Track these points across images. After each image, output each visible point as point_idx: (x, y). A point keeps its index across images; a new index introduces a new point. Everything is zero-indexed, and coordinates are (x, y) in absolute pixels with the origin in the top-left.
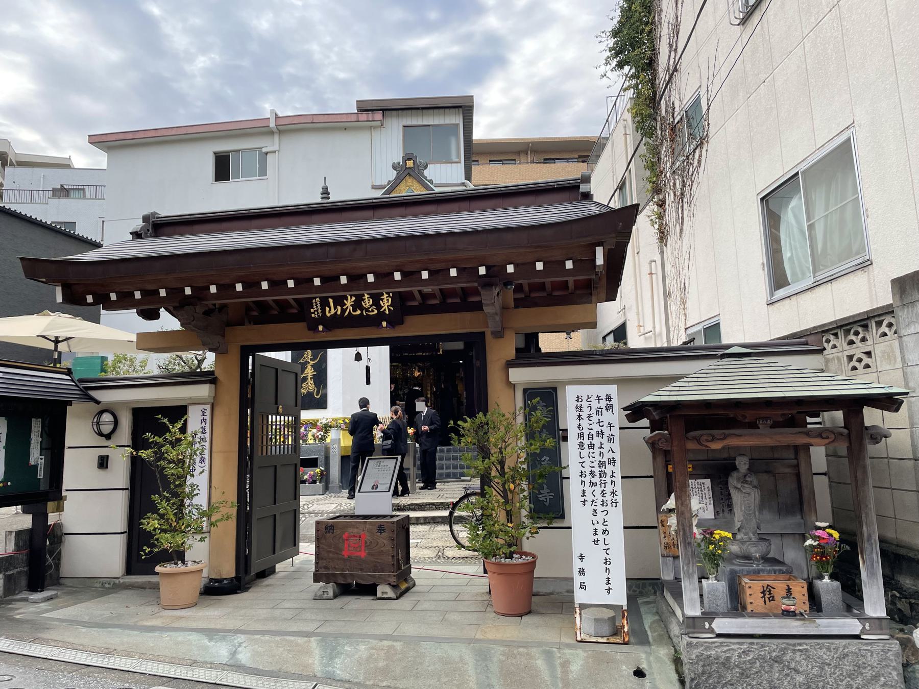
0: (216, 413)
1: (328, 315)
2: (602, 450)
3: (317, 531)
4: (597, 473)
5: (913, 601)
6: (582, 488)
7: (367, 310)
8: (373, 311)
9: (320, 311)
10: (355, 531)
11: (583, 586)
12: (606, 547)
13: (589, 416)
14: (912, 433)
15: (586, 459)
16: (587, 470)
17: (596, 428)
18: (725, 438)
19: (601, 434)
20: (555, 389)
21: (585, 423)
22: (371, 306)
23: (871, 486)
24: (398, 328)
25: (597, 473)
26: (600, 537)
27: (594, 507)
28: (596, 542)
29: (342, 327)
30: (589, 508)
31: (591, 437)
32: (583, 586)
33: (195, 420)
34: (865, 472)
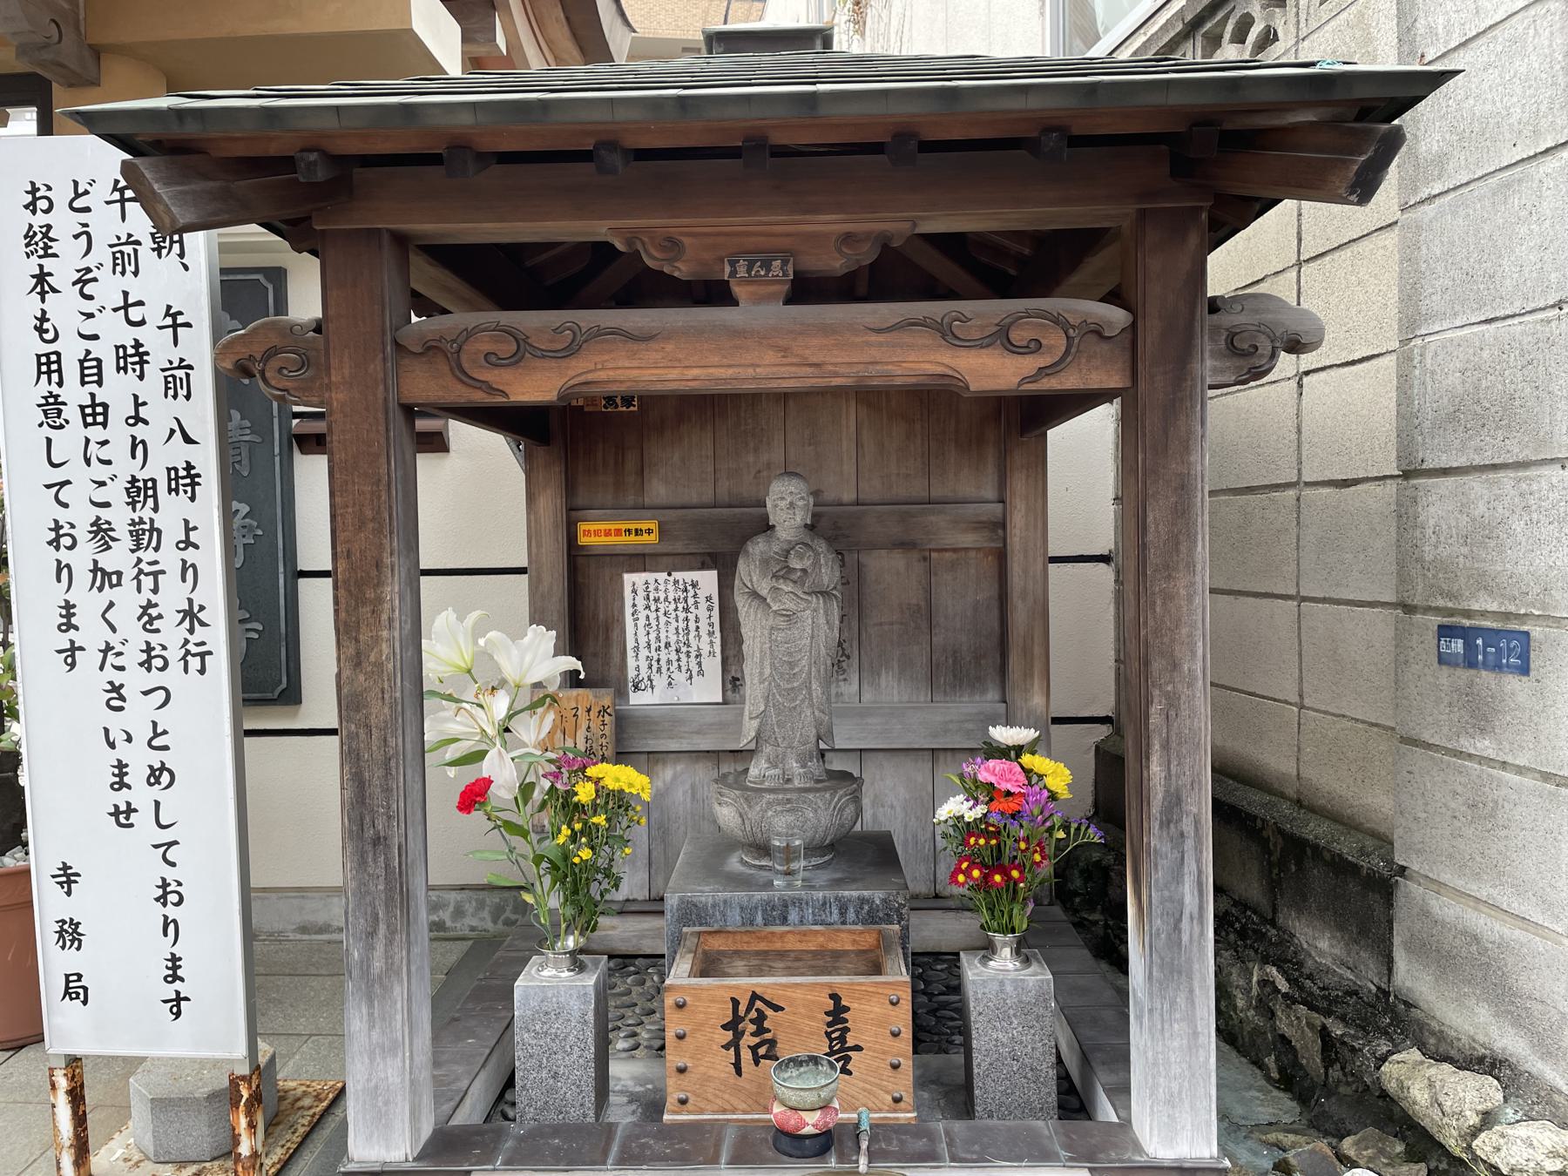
2: (140, 431)
4: (122, 530)
5: (1338, 1030)
6: (58, 594)
11: (75, 989)
12: (166, 836)
13: (84, 279)
14: (1404, 380)
15: (74, 469)
16: (81, 516)
17: (113, 331)
18: (571, 351)
19: (134, 358)
21: (64, 308)
23: (1204, 578)
25: (122, 530)
26: (141, 794)
27: (110, 674)
28: (123, 816)
30: (90, 677)
31: (91, 370)
32: (75, 989)
34: (1182, 512)
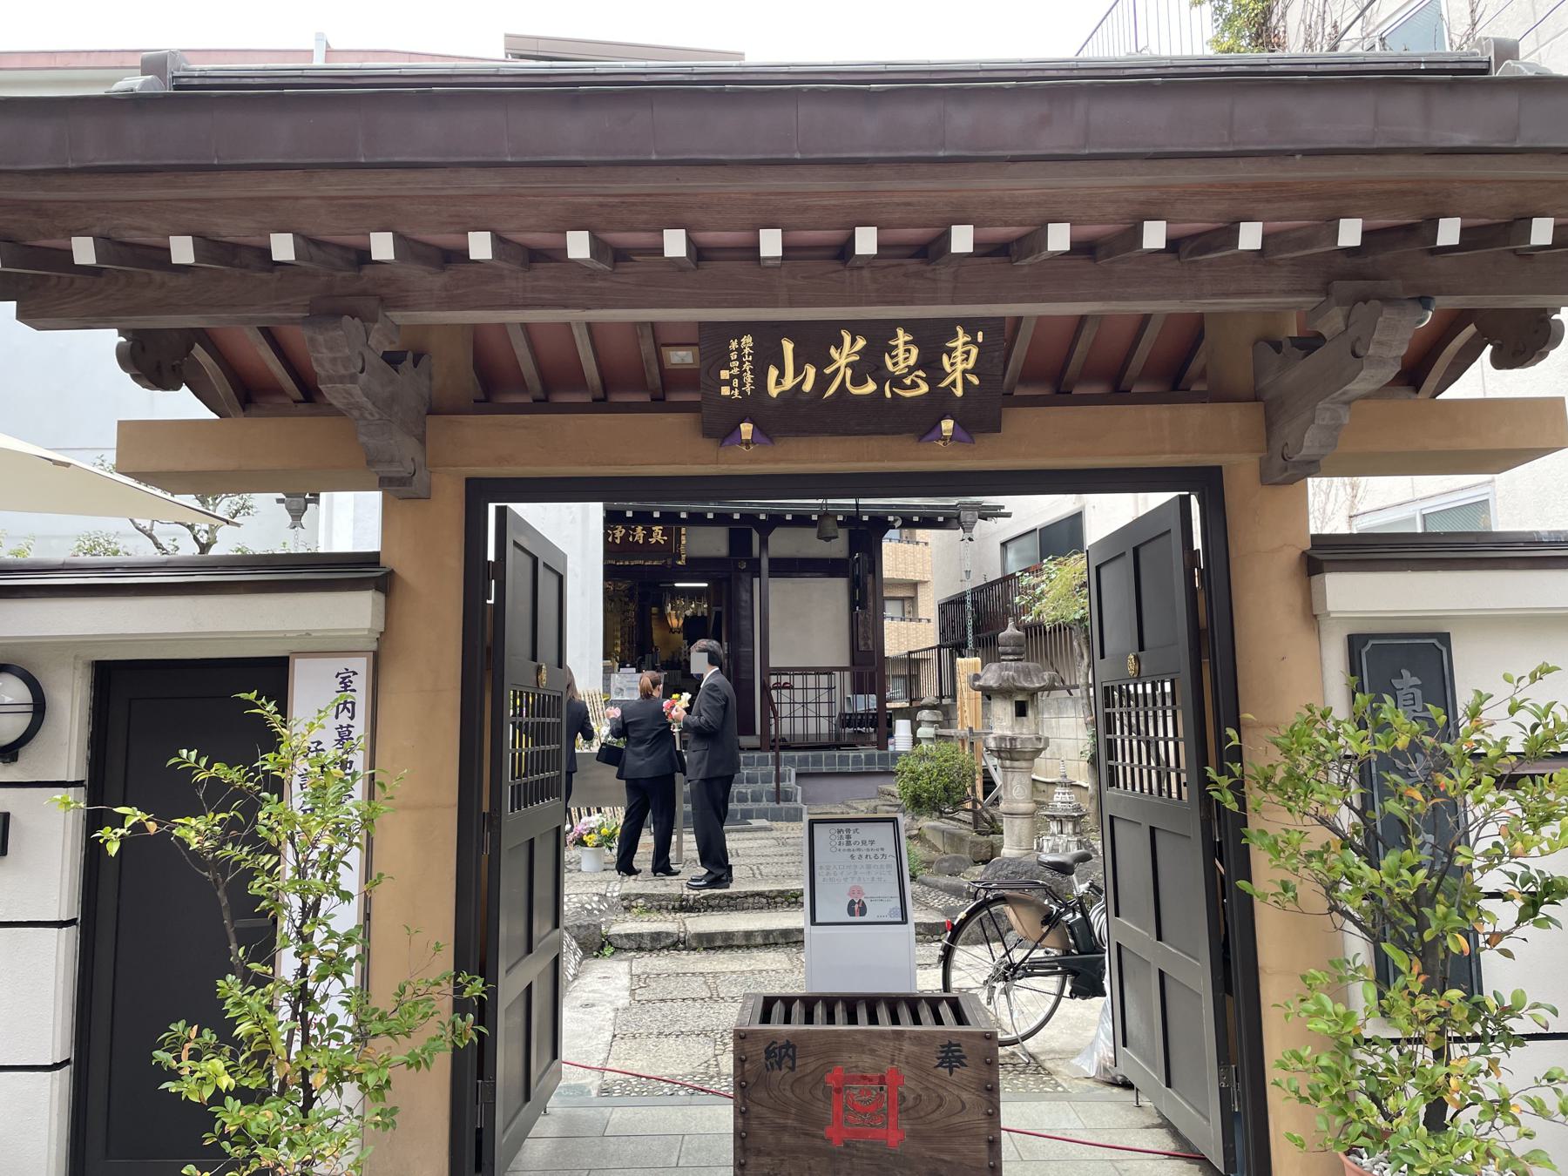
0: (390, 681)
1: (774, 391)
3: (740, 1062)
7: (897, 382)
8: (915, 385)
9: (748, 377)
10: (867, 1061)
20: (1445, 638)
22: (911, 370)
24: (986, 441)
29: (834, 432)
33: (314, 714)
